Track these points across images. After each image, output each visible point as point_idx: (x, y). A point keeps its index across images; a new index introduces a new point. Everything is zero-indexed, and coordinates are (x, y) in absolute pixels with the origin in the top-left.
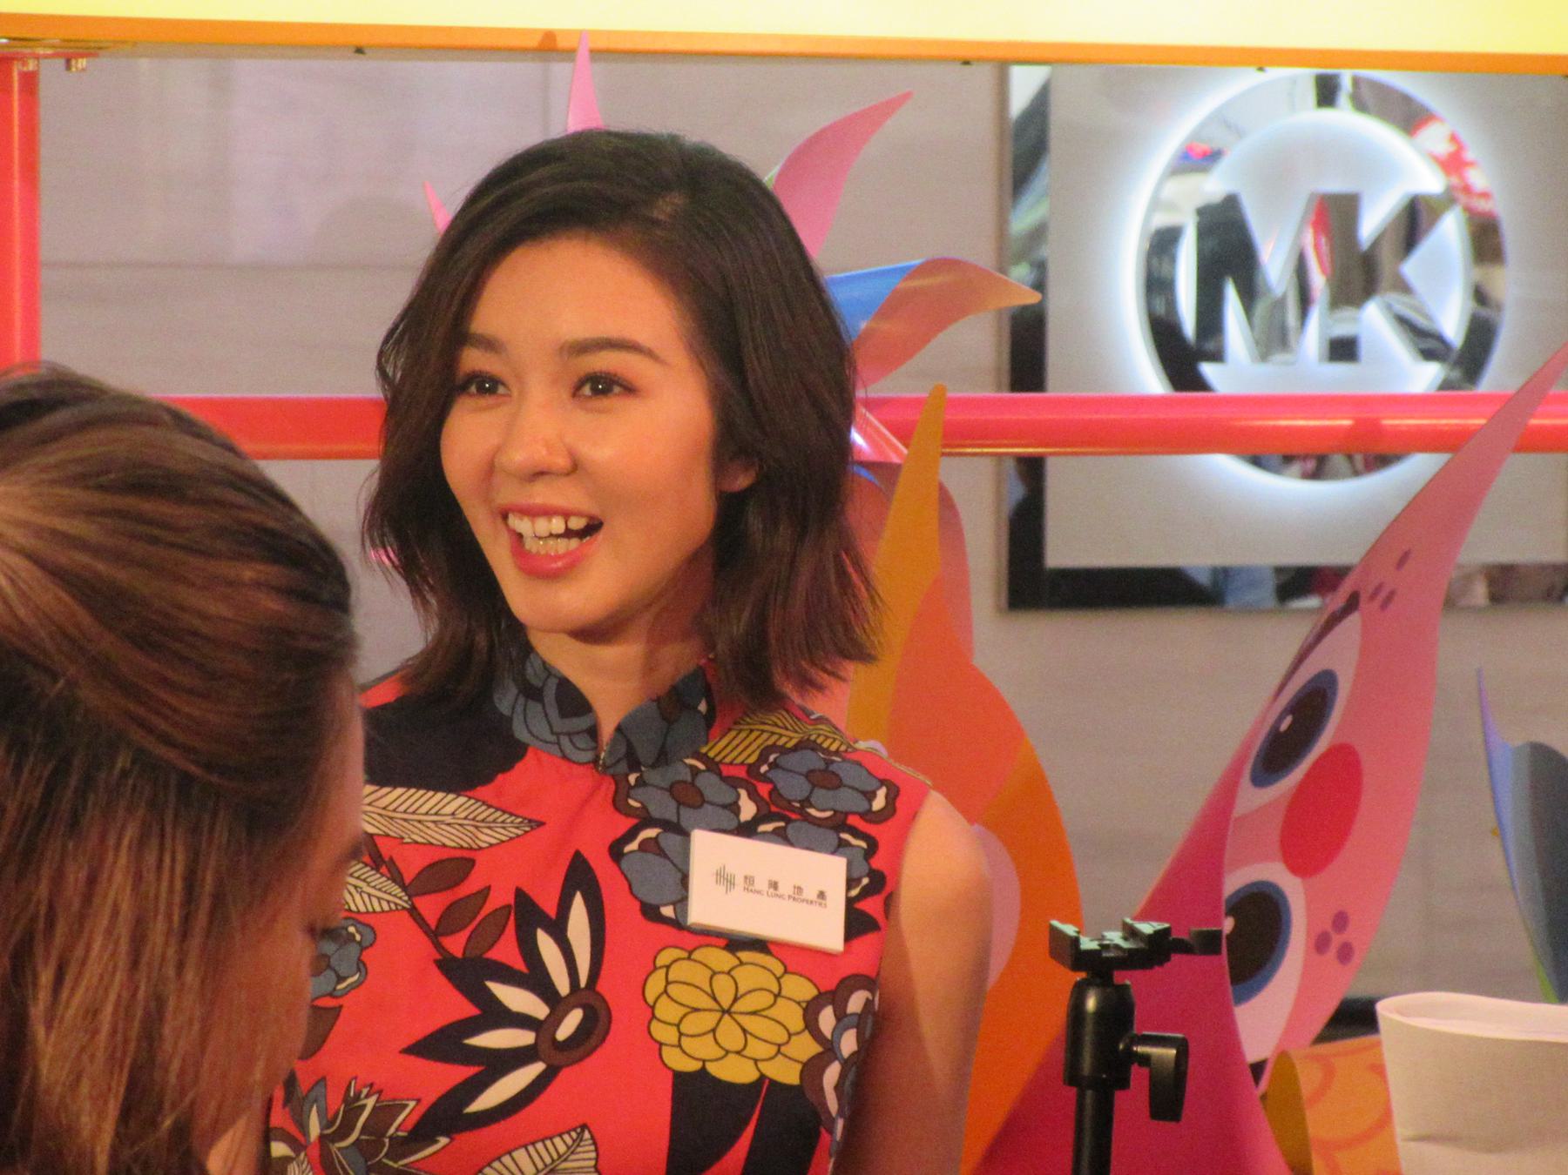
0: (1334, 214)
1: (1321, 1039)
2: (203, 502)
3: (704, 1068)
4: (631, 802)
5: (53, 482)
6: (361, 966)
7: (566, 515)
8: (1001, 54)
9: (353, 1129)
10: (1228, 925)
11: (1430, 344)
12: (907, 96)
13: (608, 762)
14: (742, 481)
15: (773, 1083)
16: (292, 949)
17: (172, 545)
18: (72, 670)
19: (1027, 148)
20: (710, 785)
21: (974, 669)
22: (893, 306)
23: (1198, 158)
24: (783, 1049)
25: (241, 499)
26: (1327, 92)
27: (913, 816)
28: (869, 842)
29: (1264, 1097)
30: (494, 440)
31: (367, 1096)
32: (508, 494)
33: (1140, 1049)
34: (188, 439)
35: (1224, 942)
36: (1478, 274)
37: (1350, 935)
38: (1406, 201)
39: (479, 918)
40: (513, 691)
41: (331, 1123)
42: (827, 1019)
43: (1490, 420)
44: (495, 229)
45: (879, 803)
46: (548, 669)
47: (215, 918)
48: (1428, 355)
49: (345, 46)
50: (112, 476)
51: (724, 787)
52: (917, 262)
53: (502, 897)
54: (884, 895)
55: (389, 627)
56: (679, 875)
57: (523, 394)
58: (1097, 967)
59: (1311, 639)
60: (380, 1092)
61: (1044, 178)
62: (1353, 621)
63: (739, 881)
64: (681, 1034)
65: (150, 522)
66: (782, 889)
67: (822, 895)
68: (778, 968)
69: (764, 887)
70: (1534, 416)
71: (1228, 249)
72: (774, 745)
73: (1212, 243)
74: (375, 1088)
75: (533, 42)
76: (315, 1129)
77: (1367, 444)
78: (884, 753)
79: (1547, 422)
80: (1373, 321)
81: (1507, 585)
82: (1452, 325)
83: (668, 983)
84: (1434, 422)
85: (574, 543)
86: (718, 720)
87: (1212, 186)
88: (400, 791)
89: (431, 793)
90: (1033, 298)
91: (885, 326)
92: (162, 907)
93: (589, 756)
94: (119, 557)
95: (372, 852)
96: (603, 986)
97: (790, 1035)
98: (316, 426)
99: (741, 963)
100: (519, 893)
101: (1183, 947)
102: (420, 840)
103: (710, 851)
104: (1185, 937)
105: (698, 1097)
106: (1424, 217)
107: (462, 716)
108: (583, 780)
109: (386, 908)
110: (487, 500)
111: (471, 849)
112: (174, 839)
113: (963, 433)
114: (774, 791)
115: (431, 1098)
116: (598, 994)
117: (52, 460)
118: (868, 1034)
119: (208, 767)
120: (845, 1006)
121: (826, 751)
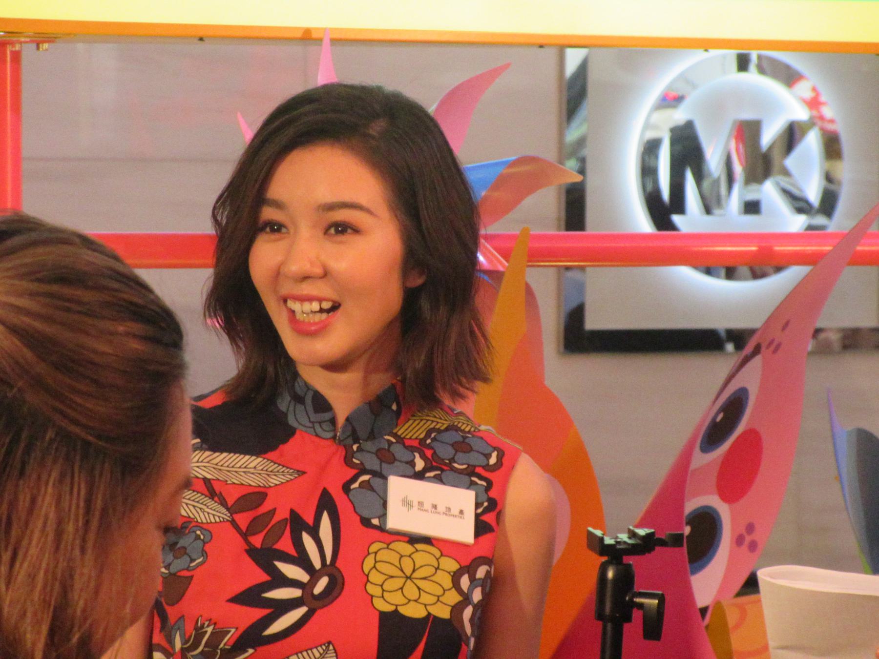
0: (747, 132)
1: (739, 594)
4: (354, 460)
5: (10, 277)
6: (204, 553)
7: (320, 300)
8: (562, 42)
10: (687, 530)
11: (801, 204)
12: (506, 66)
15: (435, 617)
16: (149, 541)
17: (79, 312)
18: (20, 384)
19: (575, 94)
20: (398, 451)
21: (545, 387)
22: (501, 182)
23: (671, 100)
25: (116, 285)
26: (743, 63)
28: (487, 482)
29: (707, 627)
30: (279, 258)
31: (208, 626)
32: (287, 288)
33: (637, 600)
34: (89, 252)
35: (685, 540)
36: (827, 165)
37: (756, 536)
38: (786, 125)
39: (270, 526)
40: (289, 398)
41: (187, 642)
42: (465, 582)
43: (835, 247)
44: (283, 138)
45: (493, 460)
46: (307, 386)
47: (104, 524)
48: (800, 211)
52: (513, 158)
53: (282, 514)
55: (211, 362)
56: (382, 501)
58: (613, 554)
60: (215, 624)
61: (585, 111)
62: (757, 361)
63: (415, 504)
64: (383, 590)
65: (68, 300)
66: (440, 509)
67: (461, 512)
69: (429, 508)
71: (688, 151)
72: (434, 428)
73: (679, 148)
74: (213, 621)
75: (299, 35)
76: (178, 645)
77: (761, 261)
78: (494, 431)
79: (866, 248)
80: (769, 191)
81: (853, 340)
82: (813, 193)
83: (376, 562)
85: (324, 316)
86: (403, 414)
87: (679, 116)
88: (225, 454)
89: (242, 456)
90: (578, 178)
91: (496, 194)
92: (72, 517)
93: (330, 435)
94: (47, 319)
95: (210, 489)
96: (338, 564)
97: (444, 591)
98: (174, 250)
100: (292, 512)
101: (662, 543)
103: (399, 487)
104: (663, 537)
105: (392, 622)
107: (257, 412)
109: (218, 520)
110: (275, 291)
111: (265, 487)
112: (79, 476)
113: (539, 254)
114: (435, 452)
115: (243, 627)
117: (10, 265)
118: (487, 589)
119: (99, 437)
121: (463, 431)
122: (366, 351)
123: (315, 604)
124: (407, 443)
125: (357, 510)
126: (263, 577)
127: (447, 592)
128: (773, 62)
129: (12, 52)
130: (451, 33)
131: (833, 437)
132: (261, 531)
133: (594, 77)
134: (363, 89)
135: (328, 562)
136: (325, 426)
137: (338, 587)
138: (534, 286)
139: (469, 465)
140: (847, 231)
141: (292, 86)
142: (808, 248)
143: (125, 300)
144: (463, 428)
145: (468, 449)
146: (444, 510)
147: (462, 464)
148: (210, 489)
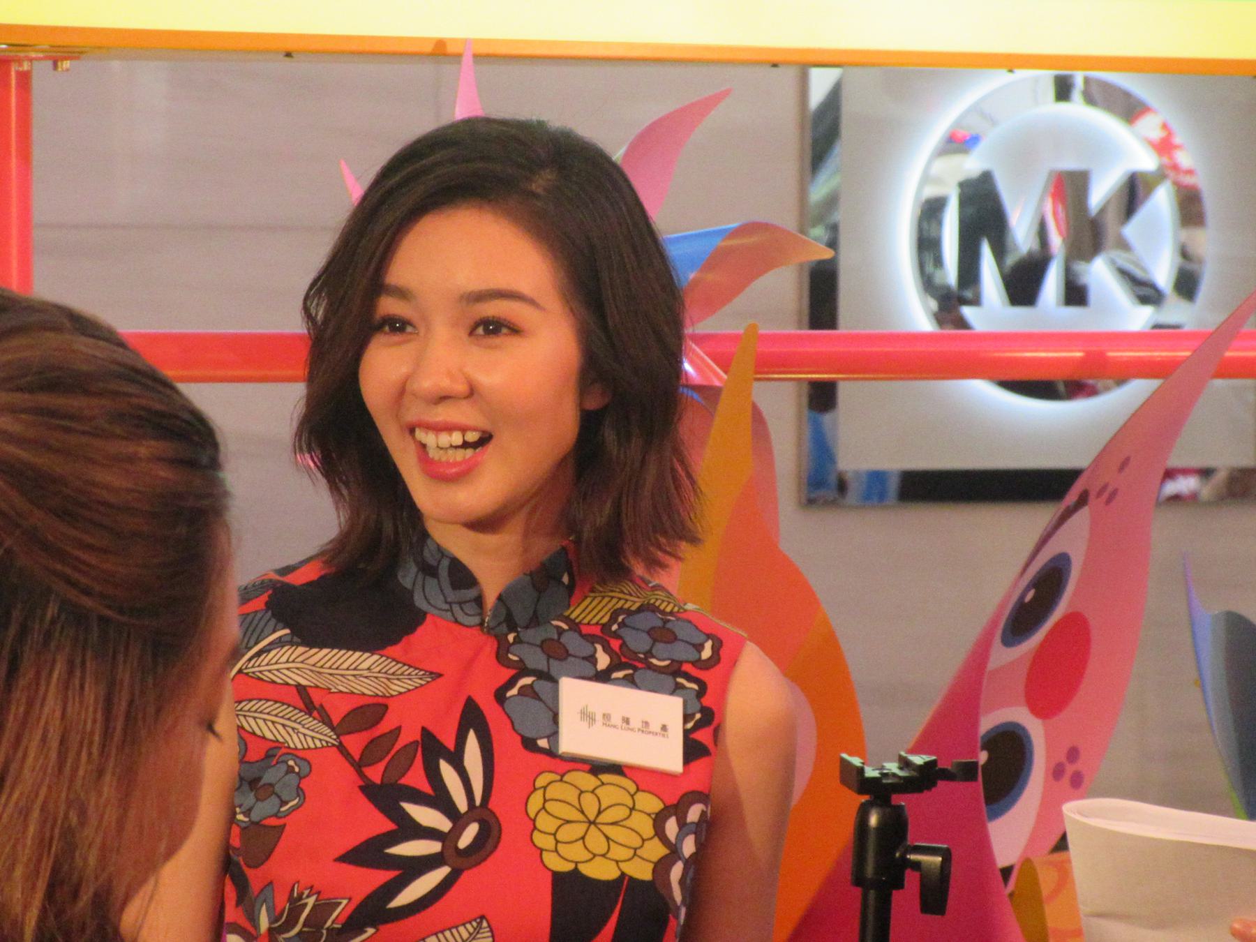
0: (1069, 187)
2: (100, 394)
3: (576, 868)
4: (511, 656)
6: (300, 791)
7: (464, 430)
9: (297, 922)
10: (983, 757)
13: (492, 625)
14: (593, 404)
15: (631, 878)
17: (84, 433)
19: (823, 133)
20: (572, 642)
22: (716, 260)
23: (958, 143)
24: (638, 852)
27: (734, 663)
28: (698, 680)
29: (1011, 895)
30: (404, 370)
31: (308, 896)
32: (414, 412)
33: (912, 857)
38: (1125, 179)
39: (393, 752)
42: (671, 827)
45: (707, 653)
48: (1144, 300)
49: (276, 52)
50: (29, 378)
51: (584, 642)
52: (735, 225)
53: (410, 735)
54: (712, 727)
57: (428, 329)
58: (878, 791)
59: (1054, 522)
60: (319, 893)
61: (840, 152)
62: (1082, 518)
63: (599, 717)
64: (557, 842)
67: (664, 728)
68: (632, 788)
69: (618, 722)
70: (1228, 349)
71: (983, 214)
73: (970, 210)
76: (264, 923)
82: (1163, 274)
83: (545, 801)
84: (1149, 354)
85: (469, 452)
86: (577, 592)
87: (971, 165)
88: (325, 651)
90: (828, 254)
91: (710, 277)
93: (477, 620)
96: (493, 804)
97: (644, 840)
98: (246, 357)
99: (603, 784)
100: (425, 731)
101: (947, 775)
102: (344, 690)
103: (575, 694)
105: (571, 889)
106: (1141, 190)
108: (476, 637)
109: (319, 745)
110: (397, 417)
111: (384, 696)
113: (770, 363)
114: (624, 644)
115: (358, 898)
116: (491, 811)
119: (121, 611)
120: (686, 817)
121: (663, 612)
122: (528, 501)
123: (461, 862)
124: (585, 630)
125: (517, 727)
126: (382, 824)
127: (646, 843)
128: (1106, 87)
129: (18, 73)
130: (645, 46)
131: (1192, 624)
132: (381, 760)
133: (849, 109)
134: (523, 126)
135: (478, 802)
136: (467, 607)
137: (491, 842)
138: (764, 408)
139: (673, 661)
140: (1212, 328)
141: (419, 123)
142: (1156, 354)
143: (143, 408)
144: (662, 607)
145: (672, 638)
146: (639, 725)
147: (664, 660)
148: (306, 700)
